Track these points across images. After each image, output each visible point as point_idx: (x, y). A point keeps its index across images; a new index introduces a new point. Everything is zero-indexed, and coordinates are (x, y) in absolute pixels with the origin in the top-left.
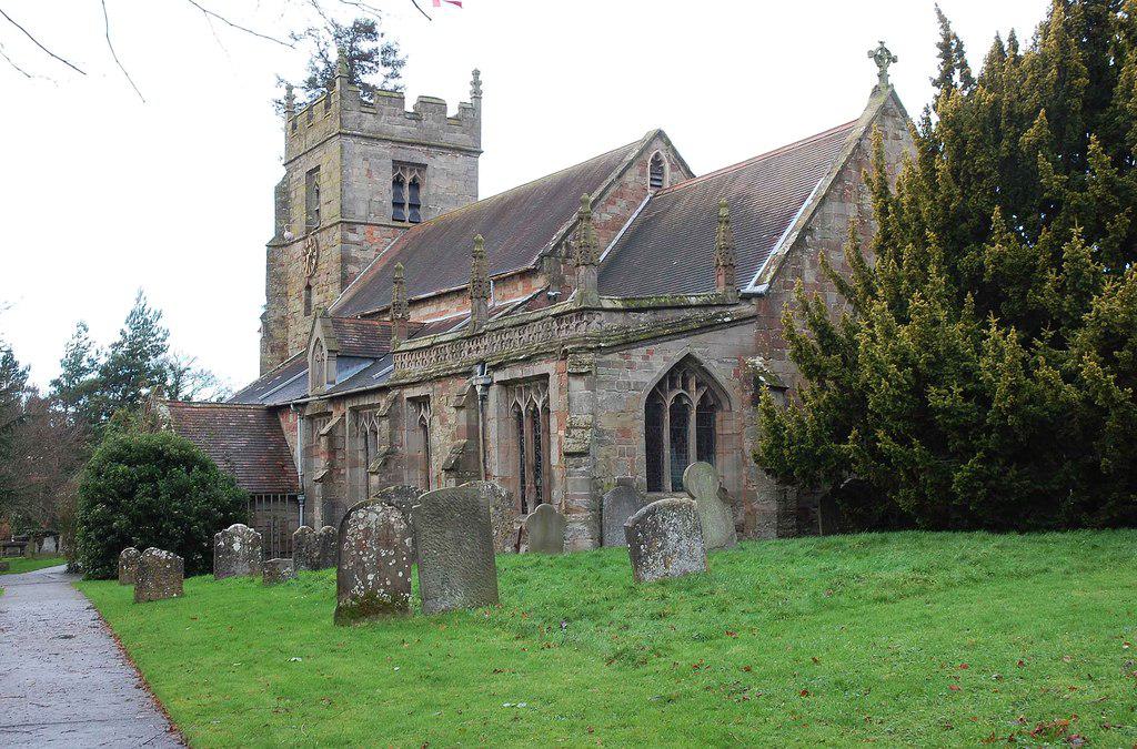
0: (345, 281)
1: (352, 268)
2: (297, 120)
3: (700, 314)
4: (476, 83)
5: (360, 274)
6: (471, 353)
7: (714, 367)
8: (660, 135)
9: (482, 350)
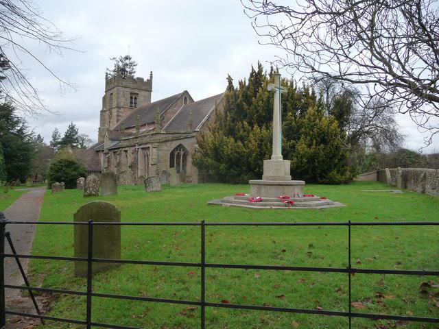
0: (118, 121)
1: (119, 118)
2: (109, 82)
3: (184, 135)
4: (151, 75)
5: (122, 119)
6: (136, 141)
7: (186, 147)
8: (186, 92)
9: (138, 141)
